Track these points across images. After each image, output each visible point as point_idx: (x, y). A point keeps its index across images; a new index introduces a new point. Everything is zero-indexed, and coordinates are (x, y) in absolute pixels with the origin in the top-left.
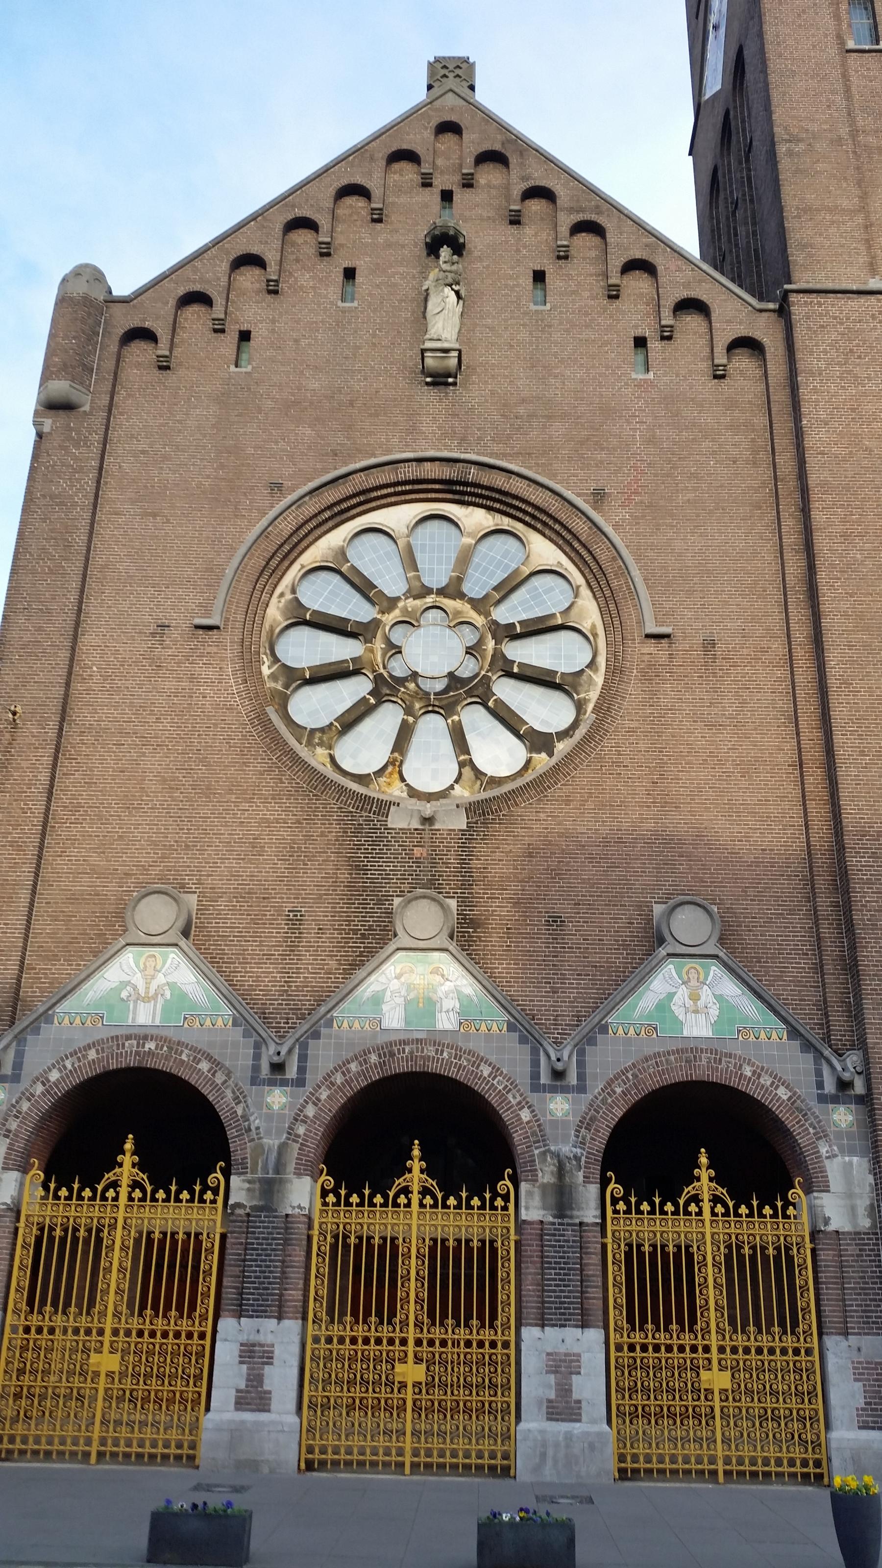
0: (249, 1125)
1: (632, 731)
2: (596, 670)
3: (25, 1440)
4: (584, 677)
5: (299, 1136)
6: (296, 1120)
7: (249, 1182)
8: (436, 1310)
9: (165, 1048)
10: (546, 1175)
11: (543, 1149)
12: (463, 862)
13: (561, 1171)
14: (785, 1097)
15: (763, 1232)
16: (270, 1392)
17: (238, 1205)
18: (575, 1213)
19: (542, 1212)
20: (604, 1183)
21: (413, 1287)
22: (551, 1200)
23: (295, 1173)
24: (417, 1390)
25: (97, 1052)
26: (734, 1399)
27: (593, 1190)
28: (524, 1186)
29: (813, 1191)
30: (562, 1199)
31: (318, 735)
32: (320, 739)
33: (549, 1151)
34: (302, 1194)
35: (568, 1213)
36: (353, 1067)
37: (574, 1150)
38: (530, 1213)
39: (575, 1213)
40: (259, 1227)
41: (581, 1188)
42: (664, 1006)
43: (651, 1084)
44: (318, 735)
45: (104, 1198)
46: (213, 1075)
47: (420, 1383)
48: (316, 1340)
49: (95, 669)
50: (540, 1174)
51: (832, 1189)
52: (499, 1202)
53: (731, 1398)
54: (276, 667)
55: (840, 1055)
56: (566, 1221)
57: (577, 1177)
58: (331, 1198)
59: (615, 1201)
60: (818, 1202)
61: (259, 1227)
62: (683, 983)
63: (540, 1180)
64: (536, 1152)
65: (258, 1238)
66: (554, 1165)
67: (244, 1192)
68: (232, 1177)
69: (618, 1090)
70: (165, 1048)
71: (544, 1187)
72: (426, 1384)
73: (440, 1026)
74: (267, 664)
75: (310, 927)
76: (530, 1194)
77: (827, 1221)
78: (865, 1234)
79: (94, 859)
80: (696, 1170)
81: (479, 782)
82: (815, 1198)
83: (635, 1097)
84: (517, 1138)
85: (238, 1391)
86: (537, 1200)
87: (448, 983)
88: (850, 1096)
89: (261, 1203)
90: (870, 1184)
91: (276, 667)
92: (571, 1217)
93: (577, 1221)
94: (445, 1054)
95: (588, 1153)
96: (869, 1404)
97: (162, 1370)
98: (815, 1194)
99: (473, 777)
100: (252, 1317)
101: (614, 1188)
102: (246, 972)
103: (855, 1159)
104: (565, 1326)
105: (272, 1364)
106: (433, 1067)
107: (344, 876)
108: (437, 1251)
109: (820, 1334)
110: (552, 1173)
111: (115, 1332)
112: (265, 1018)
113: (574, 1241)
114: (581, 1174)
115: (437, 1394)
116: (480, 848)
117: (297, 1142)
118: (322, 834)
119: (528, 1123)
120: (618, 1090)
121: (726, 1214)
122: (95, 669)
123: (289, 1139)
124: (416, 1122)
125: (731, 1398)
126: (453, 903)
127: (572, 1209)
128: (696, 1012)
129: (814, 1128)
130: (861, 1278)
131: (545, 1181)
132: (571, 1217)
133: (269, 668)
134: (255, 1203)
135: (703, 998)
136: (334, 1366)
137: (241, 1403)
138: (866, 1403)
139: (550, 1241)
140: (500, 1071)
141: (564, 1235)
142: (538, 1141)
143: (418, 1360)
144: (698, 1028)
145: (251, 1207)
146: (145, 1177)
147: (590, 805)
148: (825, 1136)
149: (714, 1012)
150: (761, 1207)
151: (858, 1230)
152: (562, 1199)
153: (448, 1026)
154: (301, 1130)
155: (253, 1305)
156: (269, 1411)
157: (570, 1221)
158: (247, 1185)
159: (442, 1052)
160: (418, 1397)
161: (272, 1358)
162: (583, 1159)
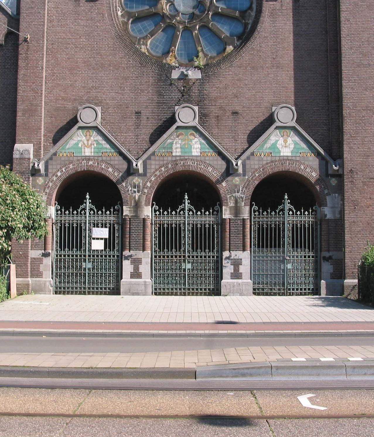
0: (128, 189)
1: (265, 37)
2: (252, 11)
3: (64, 288)
4: (247, 14)
5: (145, 193)
6: (144, 188)
7: (129, 208)
8: (194, 247)
9: (96, 164)
10: (232, 204)
11: (230, 195)
12: (200, 92)
13: (236, 202)
14: (315, 176)
15: (304, 220)
16: (141, 273)
17: (126, 215)
18: (241, 215)
19: (230, 216)
20: (251, 206)
21: (187, 240)
22: (233, 212)
23: (145, 205)
24: (189, 271)
25: (73, 165)
26: (292, 271)
27: (247, 208)
28: (224, 208)
29: (321, 206)
30: (237, 211)
31: (142, 40)
32: (143, 42)
33: (233, 196)
34: (147, 211)
35: (239, 215)
36: (163, 169)
37: (241, 195)
38: (226, 216)
39: (241, 215)
40: (134, 222)
41: (243, 207)
42: (274, 146)
43: (270, 171)
44: (142, 40)
45: (81, 214)
46: (114, 172)
47: (190, 269)
48: (155, 257)
49: (54, 17)
50: (229, 204)
51: (328, 205)
52: (215, 213)
53: (291, 271)
54: (124, 12)
55: (335, 160)
56: (238, 218)
57: (242, 204)
58: (158, 213)
59: (255, 211)
60: (323, 210)
61: (134, 222)
62: (282, 136)
63: (229, 205)
64: (228, 196)
65: (134, 226)
66: (234, 200)
67: (128, 211)
68: (124, 207)
69: (257, 175)
70: (96, 164)
71: (230, 208)
72: (192, 269)
73: (194, 154)
74: (120, 11)
75: (144, 117)
76: (226, 210)
77: (326, 216)
78: (338, 220)
79: (62, 94)
80: (283, 201)
81: (206, 59)
82: (322, 208)
83: (263, 177)
84: (221, 192)
85: (131, 273)
86: (228, 212)
87: (196, 139)
88: (325, 173)
89: (134, 215)
90: (341, 204)
91: (124, 12)
92: (240, 217)
93: (242, 218)
94: (195, 164)
95: (246, 196)
96: (334, 271)
97: (106, 267)
98: (322, 207)
99: (204, 57)
100: (134, 250)
101: (255, 207)
102: (122, 135)
103: (337, 195)
104: (237, 251)
105: (141, 264)
106: (191, 169)
107: (155, 98)
108: (195, 229)
109: (321, 251)
110: (233, 203)
111: (89, 256)
112: (130, 152)
113: (240, 224)
114: (243, 203)
115: (195, 272)
116: (207, 87)
117: (145, 195)
118: (146, 82)
119: (225, 187)
120: (257, 175)
121: (293, 214)
122: (54, 17)
123: (142, 194)
124: (183, 188)
125: (291, 271)
126: (196, 108)
127: (240, 214)
128: (286, 147)
129: (324, 185)
130: (336, 233)
131: (231, 205)
132: (240, 217)
133: (121, 12)
134: (131, 215)
135: (288, 142)
136: (158, 267)
137: (133, 276)
138: (333, 271)
139: (232, 224)
140: (213, 170)
141: (237, 223)
142: (229, 193)
143: (189, 262)
144: (286, 152)
145: (131, 216)
146: (94, 207)
147: (249, 68)
148: (327, 188)
149: (292, 146)
150: (304, 212)
151: (335, 218)
152: (237, 211)
153: (196, 154)
154: (146, 191)
155: (134, 247)
156: (141, 278)
157: (239, 218)
158: (129, 209)
159: (195, 163)
160: (189, 273)
161: (141, 262)
162: (244, 198)
